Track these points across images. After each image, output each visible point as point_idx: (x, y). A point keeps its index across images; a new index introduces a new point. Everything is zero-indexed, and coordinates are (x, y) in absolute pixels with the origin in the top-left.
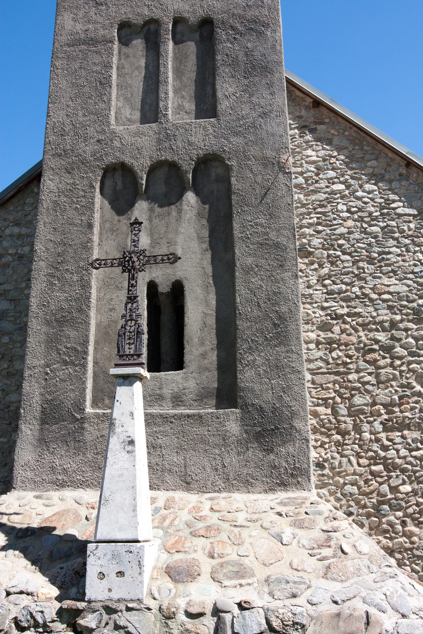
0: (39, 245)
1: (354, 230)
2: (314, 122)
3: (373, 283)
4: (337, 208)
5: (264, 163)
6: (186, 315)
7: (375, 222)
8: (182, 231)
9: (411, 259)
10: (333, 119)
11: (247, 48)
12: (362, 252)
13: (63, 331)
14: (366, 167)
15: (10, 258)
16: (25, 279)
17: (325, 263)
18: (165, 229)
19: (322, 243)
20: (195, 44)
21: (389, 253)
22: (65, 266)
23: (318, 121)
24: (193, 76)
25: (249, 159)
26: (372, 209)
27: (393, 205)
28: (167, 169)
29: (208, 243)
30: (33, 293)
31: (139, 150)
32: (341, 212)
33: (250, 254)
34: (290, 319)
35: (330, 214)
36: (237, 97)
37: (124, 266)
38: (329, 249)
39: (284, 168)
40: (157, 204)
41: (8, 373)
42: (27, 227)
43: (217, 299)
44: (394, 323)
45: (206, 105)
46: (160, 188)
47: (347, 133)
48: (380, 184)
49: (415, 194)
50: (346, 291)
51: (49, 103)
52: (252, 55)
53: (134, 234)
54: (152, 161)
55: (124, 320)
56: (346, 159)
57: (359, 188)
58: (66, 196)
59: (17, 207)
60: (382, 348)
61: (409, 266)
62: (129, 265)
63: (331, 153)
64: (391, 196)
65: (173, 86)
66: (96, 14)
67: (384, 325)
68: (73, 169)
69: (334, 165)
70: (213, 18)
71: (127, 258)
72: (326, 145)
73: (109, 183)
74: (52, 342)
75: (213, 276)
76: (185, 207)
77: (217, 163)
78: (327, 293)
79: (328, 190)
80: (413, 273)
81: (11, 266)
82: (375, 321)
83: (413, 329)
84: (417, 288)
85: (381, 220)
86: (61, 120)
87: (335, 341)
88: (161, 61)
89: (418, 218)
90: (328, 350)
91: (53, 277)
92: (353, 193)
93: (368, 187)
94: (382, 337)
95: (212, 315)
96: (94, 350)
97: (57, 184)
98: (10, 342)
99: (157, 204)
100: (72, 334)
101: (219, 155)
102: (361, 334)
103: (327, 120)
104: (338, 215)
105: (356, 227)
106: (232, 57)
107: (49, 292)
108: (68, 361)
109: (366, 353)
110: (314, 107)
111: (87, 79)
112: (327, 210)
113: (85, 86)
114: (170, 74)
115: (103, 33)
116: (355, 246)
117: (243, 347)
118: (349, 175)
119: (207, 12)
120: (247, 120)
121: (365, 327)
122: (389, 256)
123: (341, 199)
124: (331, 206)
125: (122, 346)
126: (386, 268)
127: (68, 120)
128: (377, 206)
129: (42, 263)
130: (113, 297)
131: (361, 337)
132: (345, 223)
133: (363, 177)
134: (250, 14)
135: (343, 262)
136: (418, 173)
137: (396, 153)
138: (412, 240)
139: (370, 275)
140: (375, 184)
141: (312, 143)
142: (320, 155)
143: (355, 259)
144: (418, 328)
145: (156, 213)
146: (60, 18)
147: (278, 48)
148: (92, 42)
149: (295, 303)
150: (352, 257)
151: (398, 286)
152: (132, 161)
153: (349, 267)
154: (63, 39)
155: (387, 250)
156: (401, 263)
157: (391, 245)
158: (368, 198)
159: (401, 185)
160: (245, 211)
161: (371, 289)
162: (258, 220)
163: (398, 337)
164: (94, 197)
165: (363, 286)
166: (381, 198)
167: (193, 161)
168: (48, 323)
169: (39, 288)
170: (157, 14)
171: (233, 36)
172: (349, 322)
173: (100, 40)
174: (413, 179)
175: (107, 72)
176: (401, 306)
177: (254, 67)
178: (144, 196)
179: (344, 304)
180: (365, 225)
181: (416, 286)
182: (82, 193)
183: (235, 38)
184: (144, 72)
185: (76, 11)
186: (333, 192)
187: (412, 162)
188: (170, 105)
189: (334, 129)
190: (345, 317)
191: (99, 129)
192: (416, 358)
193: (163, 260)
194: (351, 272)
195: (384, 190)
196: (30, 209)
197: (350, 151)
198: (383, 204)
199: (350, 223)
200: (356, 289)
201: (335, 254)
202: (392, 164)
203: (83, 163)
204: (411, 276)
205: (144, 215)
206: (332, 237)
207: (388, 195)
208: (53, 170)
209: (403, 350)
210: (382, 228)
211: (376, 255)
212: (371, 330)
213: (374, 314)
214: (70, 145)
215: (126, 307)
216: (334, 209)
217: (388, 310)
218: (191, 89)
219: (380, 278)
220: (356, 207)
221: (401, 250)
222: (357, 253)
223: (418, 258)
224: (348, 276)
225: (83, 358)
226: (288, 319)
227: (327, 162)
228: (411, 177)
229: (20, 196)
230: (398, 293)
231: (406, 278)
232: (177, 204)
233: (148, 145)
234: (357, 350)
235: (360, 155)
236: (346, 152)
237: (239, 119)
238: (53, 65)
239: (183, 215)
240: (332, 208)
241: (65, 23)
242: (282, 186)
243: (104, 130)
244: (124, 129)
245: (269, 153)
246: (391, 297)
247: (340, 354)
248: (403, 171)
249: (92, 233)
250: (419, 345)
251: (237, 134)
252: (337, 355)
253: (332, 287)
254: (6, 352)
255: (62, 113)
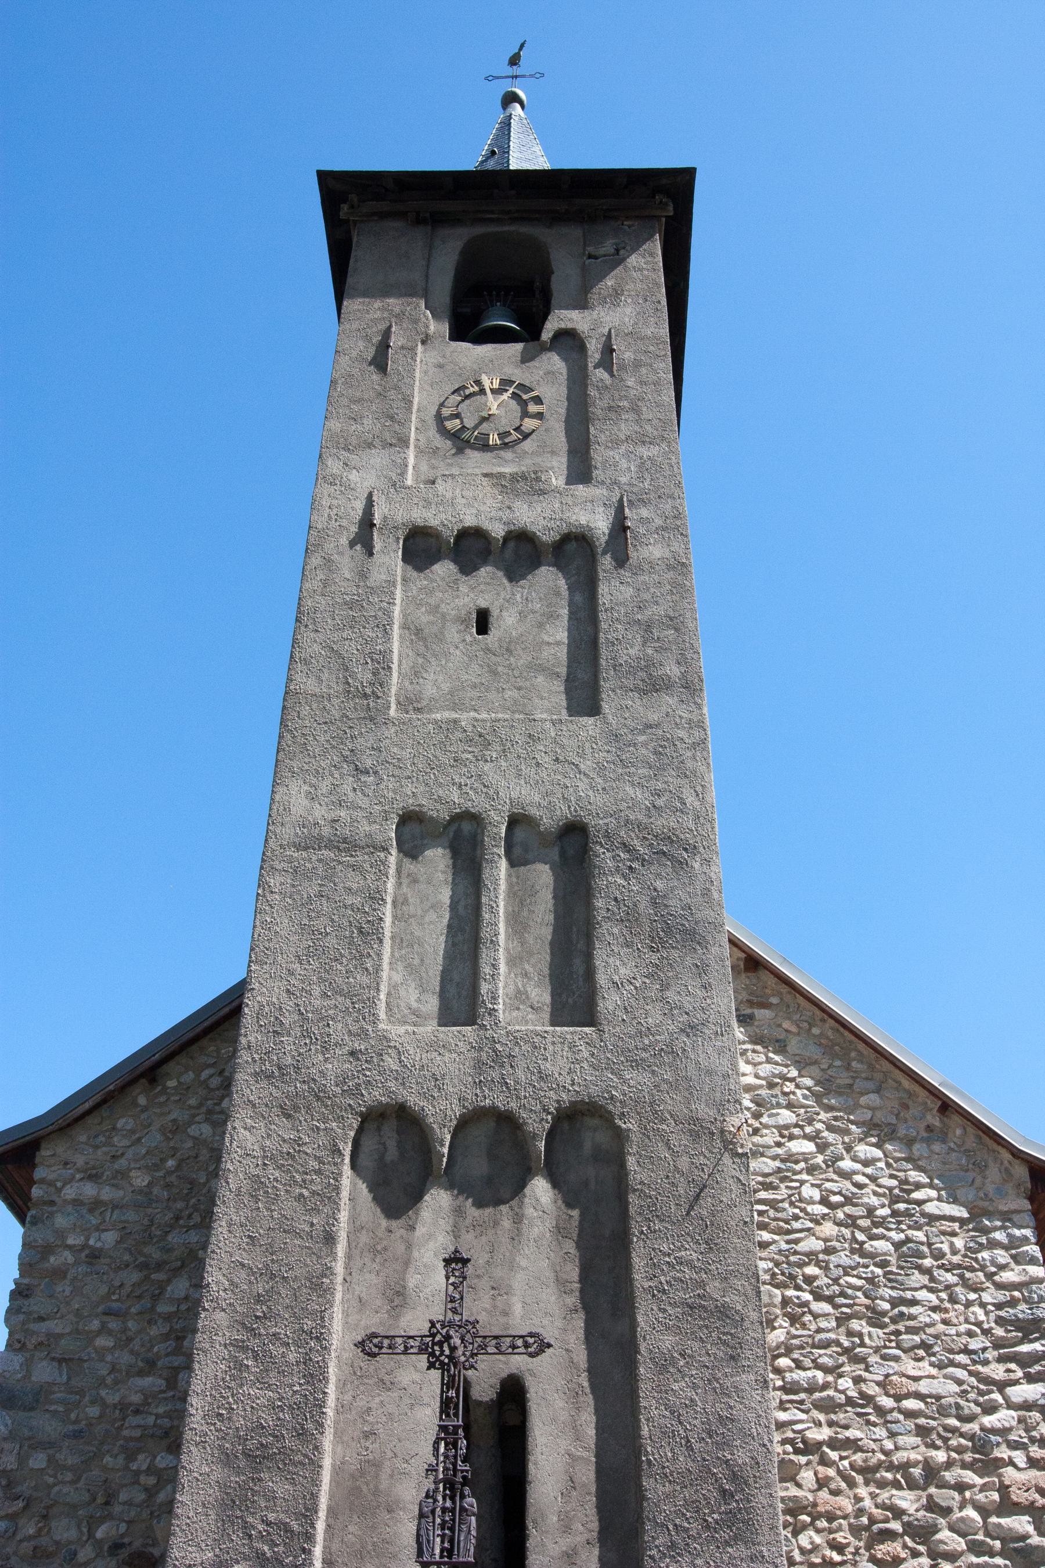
0: (214, 1274)
1: (837, 1245)
2: (748, 1001)
3: (883, 1371)
4: (799, 1194)
5: (694, 1130)
6: (531, 1458)
7: (880, 1230)
8: (524, 1263)
9: (962, 1319)
10: (788, 998)
11: (655, 889)
12: (857, 1297)
13: (260, 1480)
14: (857, 1106)
15: (68, 1257)
16: (100, 1309)
17: (777, 1317)
18: (487, 1256)
19: (770, 1269)
20: (551, 868)
21: (914, 1302)
22: (271, 1327)
23: (755, 1000)
24: (547, 932)
25: (663, 1120)
26: (874, 1201)
27: (916, 1195)
28: (492, 1124)
29: (578, 1294)
30: (197, 1384)
31: (437, 1080)
32: (808, 1204)
33: (668, 1328)
34: (756, 1482)
35: (786, 1205)
36: (636, 988)
37: (432, 1354)
38: (786, 1287)
39: (734, 1144)
40: (470, 1200)
41: (35, 1548)
42: (116, 1186)
43: (597, 1423)
44: (932, 1469)
45: (574, 999)
46: (478, 1166)
47: (816, 1031)
48: (889, 1147)
49: (962, 1173)
50: (825, 1386)
51: (250, 961)
52: (666, 906)
53: (452, 1284)
54: (464, 1107)
55: (432, 1478)
56: (816, 1085)
57: (844, 1153)
58: (279, 1167)
59: (96, 1136)
60: (909, 1529)
61: (958, 1335)
62: (442, 1352)
63: (785, 1070)
64: (912, 1173)
65: (507, 949)
66: (355, 790)
67: (911, 1474)
68: (296, 1108)
69: (792, 1096)
70: (587, 824)
71: (438, 1338)
72: (774, 1053)
73: (369, 1144)
74: (233, 1506)
75: (590, 1371)
76: (529, 1211)
77: (595, 1122)
78: (783, 1388)
79: (779, 1151)
80: (966, 1351)
81: (69, 1276)
82: (891, 1462)
83: (974, 1486)
84: (977, 1388)
85: (894, 1226)
86: (274, 1000)
87: (806, 1507)
88: (484, 900)
89: (971, 1226)
90: (790, 1529)
91: (244, 1349)
92: (834, 1163)
93: (864, 1150)
94: (907, 1501)
95: (587, 1460)
96: (326, 1531)
97: (260, 1139)
98: (48, 1466)
99: (470, 1200)
100: (281, 1488)
101: (601, 1106)
102: (862, 1491)
103: (774, 1000)
104: (803, 1210)
105: (840, 1238)
106: (625, 905)
107: (233, 1384)
108: (268, 1555)
109: (874, 1540)
110: (747, 969)
111: (332, 921)
112: (779, 1197)
113: (327, 934)
114: (502, 927)
115: (367, 829)
116: (841, 1281)
117: (657, 1542)
118: (824, 1122)
119: (576, 811)
120: (658, 1037)
121: (869, 1476)
122: (914, 1310)
123: (808, 1173)
124: (787, 1187)
125: (428, 1541)
126: (910, 1336)
127: (291, 1003)
128: (884, 1195)
129: (219, 1315)
130: (373, 1405)
131: (861, 1500)
132: (818, 1228)
133: (853, 1127)
134: (660, 823)
135: (816, 1316)
136: (964, 1128)
137: (917, 1082)
138: (961, 1276)
139: (875, 1352)
140: (878, 1146)
141: (744, 1047)
142: (762, 1074)
143: (842, 1313)
144: (984, 1485)
145: (468, 1221)
146: (281, 789)
147: (716, 895)
148: (346, 845)
149: (764, 1445)
150: (836, 1307)
151: (935, 1381)
152: (421, 1104)
153: (829, 1331)
154: (287, 833)
155: (908, 1295)
156: (941, 1327)
157: (918, 1285)
158: (864, 1174)
159: (931, 1151)
160: (655, 1231)
161: (878, 1383)
162: (683, 1253)
163: (944, 1504)
164: (340, 1174)
165: (860, 1376)
166: (892, 1176)
167: (549, 1113)
168: (227, 1460)
169: (211, 1375)
170: (477, 803)
171: (628, 863)
172: (834, 1462)
173: (362, 843)
174: (955, 1140)
175: (375, 910)
176: (946, 1428)
177: (668, 930)
178: (444, 1179)
179: (822, 1417)
180: (861, 1237)
181: (976, 1383)
182: (313, 1164)
183: (630, 867)
184: (447, 916)
185: (314, 781)
186: (791, 1158)
187: (951, 1103)
188: (501, 992)
189: (789, 1019)
190: (825, 1449)
191: (354, 1028)
192: (986, 1558)
193: (514, 1347)
194: (833, 1341)
195: (897, 1160)
196: (126, 1142)
197: (823, 1070)
198: (896, 1191)
199: (828, 1229)
200: (845, 1383)
201: (798, 1298)
202: (910, 1103)
203: (318, 1098)
204: (962, 1358)
205: (442, 1222)
206: (792, 1258)
207: (905, 1171)
208: (254, 1106)
209: (955, 1535)
210: (898, 1245)
211: (886, 1306)
212: (882, 1484)
213: (889, 1445)
214: (293, 1057)
215: (436, 1449)
216: (793, 1195)
217: (917, 1435)
218: (543, 958)
219: (896, 1359)
220: (840, 1193)
221: (938, 1297)
222: (845, 1298)
223: (976, 1318)
224: (828, 1351)
225: (304, 1550)
226: (751, 1481)
227: (777, 1091)
228: (950, 1135)
229: (104, 1112)
230: (938, 1398)
231: (952, 1363)
232: (513, 1203)
233: (457, 1073)
234: (856, 1531)
235: (844, 1079)
236: (814, 1070)
237: (641, 1033)
238: (262, 883)
239: (525, 1230)
240: (790, 1192)
241: (292, 801)
242: (731, 1181)
243: (365, 1032)
244: (407, 1032)
245: (704, 1111)
246: (922, 1405)
247: (818, 1539)
248: (934, 1119)
249: (333, 1255)
250: (990, 1527)
251: (636, 1064)
252: (812, 1543)
253: (794, 1376)
254: (35, 1494)
255: (278, 988)
